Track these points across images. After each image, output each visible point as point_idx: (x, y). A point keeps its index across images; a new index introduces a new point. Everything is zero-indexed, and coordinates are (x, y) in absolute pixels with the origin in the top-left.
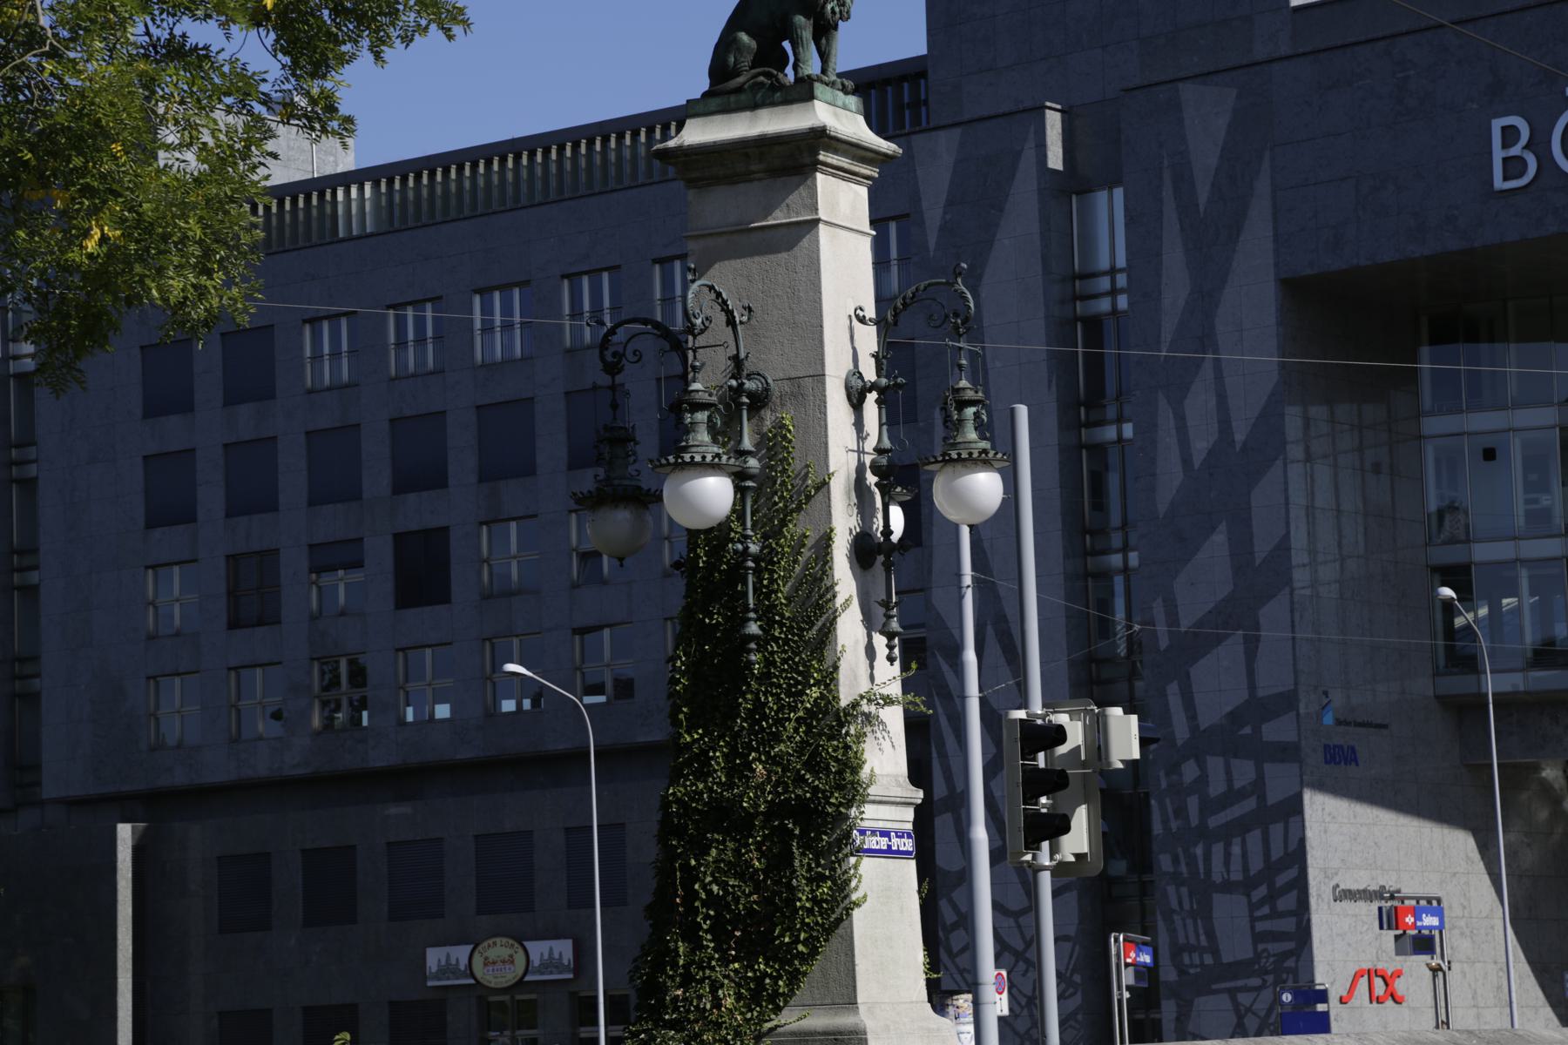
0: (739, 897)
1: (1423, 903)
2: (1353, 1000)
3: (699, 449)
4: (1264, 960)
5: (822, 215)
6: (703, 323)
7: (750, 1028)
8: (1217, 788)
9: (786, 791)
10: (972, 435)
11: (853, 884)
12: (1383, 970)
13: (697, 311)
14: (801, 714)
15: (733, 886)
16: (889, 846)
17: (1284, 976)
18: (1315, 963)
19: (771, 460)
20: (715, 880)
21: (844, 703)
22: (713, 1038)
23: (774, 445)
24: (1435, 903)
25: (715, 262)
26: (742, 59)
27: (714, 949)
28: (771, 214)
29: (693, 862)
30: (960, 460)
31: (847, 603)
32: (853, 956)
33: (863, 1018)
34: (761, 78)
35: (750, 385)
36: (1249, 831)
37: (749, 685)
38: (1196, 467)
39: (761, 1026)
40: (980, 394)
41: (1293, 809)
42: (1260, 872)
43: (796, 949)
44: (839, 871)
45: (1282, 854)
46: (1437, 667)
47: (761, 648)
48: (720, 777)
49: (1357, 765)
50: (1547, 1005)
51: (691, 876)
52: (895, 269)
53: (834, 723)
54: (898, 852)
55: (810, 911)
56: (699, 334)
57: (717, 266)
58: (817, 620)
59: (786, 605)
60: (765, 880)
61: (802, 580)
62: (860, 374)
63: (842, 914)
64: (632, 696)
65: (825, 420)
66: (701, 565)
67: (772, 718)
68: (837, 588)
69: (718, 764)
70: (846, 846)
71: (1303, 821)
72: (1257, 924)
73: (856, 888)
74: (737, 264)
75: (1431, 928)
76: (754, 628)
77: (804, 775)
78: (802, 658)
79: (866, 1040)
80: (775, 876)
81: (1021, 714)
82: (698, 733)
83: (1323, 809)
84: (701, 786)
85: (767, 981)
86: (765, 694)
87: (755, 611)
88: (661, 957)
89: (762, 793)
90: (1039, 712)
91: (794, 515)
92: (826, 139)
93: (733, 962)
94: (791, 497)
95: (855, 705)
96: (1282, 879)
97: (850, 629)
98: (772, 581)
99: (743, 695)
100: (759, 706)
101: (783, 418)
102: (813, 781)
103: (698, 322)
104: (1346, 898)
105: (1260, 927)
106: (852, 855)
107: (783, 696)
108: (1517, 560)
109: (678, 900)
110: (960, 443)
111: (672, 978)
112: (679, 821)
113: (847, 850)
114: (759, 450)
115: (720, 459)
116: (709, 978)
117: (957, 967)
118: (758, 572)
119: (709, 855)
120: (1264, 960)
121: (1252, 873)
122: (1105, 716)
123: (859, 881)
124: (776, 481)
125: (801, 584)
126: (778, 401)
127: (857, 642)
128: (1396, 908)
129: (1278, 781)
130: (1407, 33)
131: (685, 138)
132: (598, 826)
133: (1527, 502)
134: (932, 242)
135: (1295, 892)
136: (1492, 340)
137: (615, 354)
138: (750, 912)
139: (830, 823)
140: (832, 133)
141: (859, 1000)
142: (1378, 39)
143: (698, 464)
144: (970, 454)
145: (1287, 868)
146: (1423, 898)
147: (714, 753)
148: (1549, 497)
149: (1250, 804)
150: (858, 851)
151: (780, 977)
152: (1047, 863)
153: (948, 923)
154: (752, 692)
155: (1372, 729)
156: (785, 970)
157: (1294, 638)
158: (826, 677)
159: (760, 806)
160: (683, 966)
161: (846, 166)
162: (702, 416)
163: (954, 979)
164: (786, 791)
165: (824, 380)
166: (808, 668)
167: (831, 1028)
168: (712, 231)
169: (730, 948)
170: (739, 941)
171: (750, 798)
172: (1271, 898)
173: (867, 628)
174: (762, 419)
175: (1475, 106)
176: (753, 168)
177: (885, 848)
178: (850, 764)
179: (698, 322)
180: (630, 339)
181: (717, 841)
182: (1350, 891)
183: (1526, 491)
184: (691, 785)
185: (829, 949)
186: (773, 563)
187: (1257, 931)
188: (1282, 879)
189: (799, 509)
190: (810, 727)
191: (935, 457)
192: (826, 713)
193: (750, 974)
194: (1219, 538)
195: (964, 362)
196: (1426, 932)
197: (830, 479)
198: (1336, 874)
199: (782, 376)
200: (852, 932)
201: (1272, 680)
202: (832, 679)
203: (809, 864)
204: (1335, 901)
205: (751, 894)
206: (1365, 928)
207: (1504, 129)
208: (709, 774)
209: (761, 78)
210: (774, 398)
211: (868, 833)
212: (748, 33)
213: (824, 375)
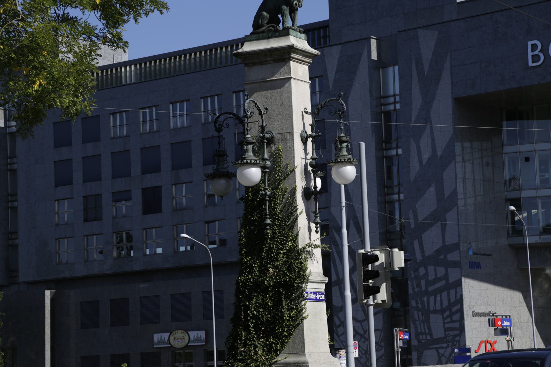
0: (263, 315)
1: (504, 317)
5: (292, 76)
7: (267, 362)
8: (431, 277)
9: (280, 278)
10: (345, 153)
11: (304, 311)
12: (490, 341)
13: (249, 110)
14: (285, 251)
15: (261, 312)
16: (316, 298)
18: (466, 339)
19: (274, 162)
20: (255, 310)
21: (300, 247)
23: (276, 157)
24: (508, 317)
25: (254, 93)
29: (247, 303)
30: (341, 162)
31: (301, 212)
32: (304, 336)
34: (271, 28)
36: (443, 292)
37: (267, 241)
38: (424, 164)
39: (271, 361)
40: (348, 139)
41: (459, 284)
42: (447, 306)
43: (284, 334)
44: (298, 306)
46: (509, 234)
48: (257, 274)
49: (481, 269)
51: (247, 308)
52: (318, 95)
53: (297, 254)
54: (319, 300)
55: (288, 321)
56: (249, 118)
57: (255, 94)
58: (291, 218)
59: (280, 213)
60: (273, 310)
62: (306, 131)
63: (300, 321)
65: (294, 148)
66: (250, 199)
67: (275, 253)
68: (298, 207)
69: (256, 269)
70: (301, 297)
71: (462, 288)
73: (305, 312)
74: (262, 93)
75: (507, 326)
76: (268, 221)
77: (286, 273)
78: (285, 232)
80: (276, 308)
81: (362, 251)
82: (249, 258)
84: (250, 277)
85: (274, 345)
86: (273, 244)
88: (236, 336)
90: (369, 250)
91: (283, 181)
92: (294, 49)
93: (262, 338)
94: (282, 175)
95: (304, 248)
96: (454, 309)
97: (302, 221)
98: (275, 204)
99: (265, 244)
100: (270, 248)
101: (279, 147)
102: (290, 275)
103: (249, 113)
104: (488, 316)
106: (303, 301)
107: (279, 245)
108: (536, 197)
109: (242, 317)
110: (341, 156)
111: (240, 344)
112: (242, 289)
113: (301, 299)
116: (253, 344)
117: (340, 340)
118: (270, 201)
119: (253, 301)
123: (306, 310)
125: (285, 205)
127: (305, 226)
128: (495, 319)
129: (453, 274)
130: (498, 11)
131: (244, 49)
132: (214, 291)
133: (540, 176)
134: (331, 86)
135: (459, 314)
137: (219, 125)
141: (306, 352)
142: (488, 14)
143: (249, 163)
144: (345, 160)
147: (255, 265)
149: (443, 282)
151: (278, 344)
152: (372, 303)
153: (337, 325)
154: (268, 244)
155: (486, 256)
156: (280, 341)
160: (244, 340)
161: (301, 58)
162: (250, 147)
163: (339, 344)
164: (280, 278)
165: (293, 134)
166: (288, 235)
169: (260, 334)
170: (263, 331)
171: (267, 281)
172: (451, 316)
173: (308, 221)
176: (268, 59)
177: (315, 298)
178: (303, 268)
179: (249, 113)
181: (256, 296)
182: (478, 313)
183: (540, 172)
184: (247, 276)
185: (295, 334)
186: (275, 198)
188: (454, 309)
189: (284, 179)
190: (288, 256)
191: (332, 161)
192: (294, 251)
193: (267, 343)
194: (432, 189)
195: (342, 127)
196: (505, 327)
197: (295, 168)
198: (473, 307)
199: (278, 132)
200: (303, 328)
201: (451, 239)
203: (288, 304)
204: (473, 316)
205: (268, 315)
206: (484, 326)
207: (532, 45)
208: (253, 272)
209: (271, 28)
210: (275, 140)
212: (266, 12)
213: (293, 132)
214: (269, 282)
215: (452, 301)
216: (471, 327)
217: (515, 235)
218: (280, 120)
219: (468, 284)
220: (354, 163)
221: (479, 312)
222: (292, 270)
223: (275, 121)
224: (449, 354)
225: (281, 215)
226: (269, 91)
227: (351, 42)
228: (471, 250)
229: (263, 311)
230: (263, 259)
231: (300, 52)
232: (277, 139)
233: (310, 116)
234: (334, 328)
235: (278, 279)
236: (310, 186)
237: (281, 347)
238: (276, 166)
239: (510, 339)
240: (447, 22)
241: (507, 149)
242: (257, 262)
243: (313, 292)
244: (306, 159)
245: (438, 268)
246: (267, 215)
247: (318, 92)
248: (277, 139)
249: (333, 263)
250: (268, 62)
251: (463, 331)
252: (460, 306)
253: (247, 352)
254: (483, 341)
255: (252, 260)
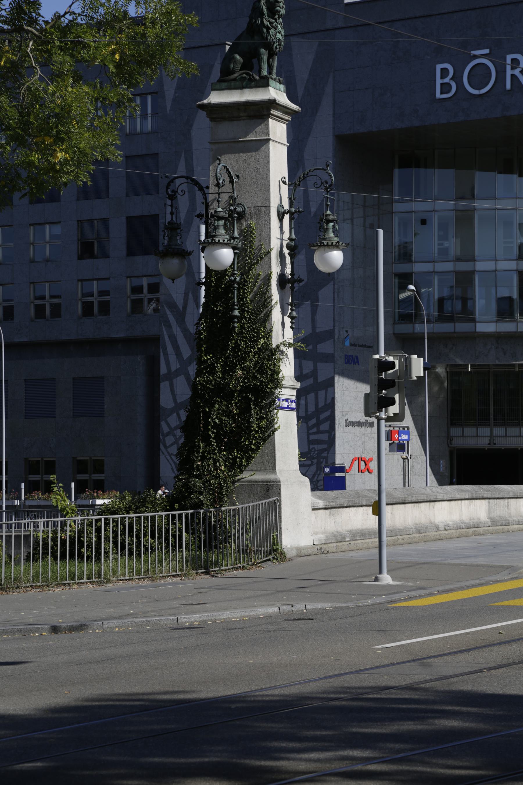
0: (227, 425)
1: (401, 429)
2: (351, 471)
3: (221, 237)
4: (313, 453)
5: (271, 137)
6: (222, 182)
7: (230, 479)
9: (249, 382)
10: (332, 235)
11: (276, 421)
12: (364, 458)
13: (220, 177)
14: (256, 350)
15: (225, 420)
16: (288, 406)
17: (322, 460)
18: (336, 454)
19: (245, 241)
20: (217, 418)
21: (274, 346)
22: (215, 482)
23: (247, 235)
24: (406, 429)
26: (237, 66)
27: (216, 446)
28: (248, 135)
29: (207, 410)
33: (278, 476)
34: (245, 75)
35: (239, 209)
36: (309, 394)
37: (233, 337)
39: (235, 478)
40: (336, 218)
41: (330, 384)
42: (313, 412)
43: (251, 447)
44: (270, 415)
45: (323, 404)
46: (395, 320)
47: (239, 321)
48: (219, 375)
49: (359, 364)
50: (432, 474)
51: (207, 415)
52: (149, 119)
53: (270, 354)
54: (291, 408)
55: (257, 432)
56: (221, 187)
58: (264, 311)
59: (250, 304)
60: (238, 418)
61: (257, 293)
62: (283, 206)
63: (270, 433)
64: (12, 319)
65: (270, 226)
66: (213, 285)
68: (273, 297)
69: (219, 369)
70: (273, 405)
71: (334, 390)
72: (310, 436)
73: (277, 423)
74: (232, 156)
75: (403, 440)
76: (236, 313)
77: (257, 375)
78: (256, 326)
79: (280, 485)
80: (242, 417)
81: (377, 357)
82: (210, 356)
83: (343, 384)
84: (211, 378)
85: (238, 460)
86: (240, 341)
87: (237, 305)
89: (238, 382)
90: (383, 356)
91: (256, 265)
92: (275, 105)
94: (254, 258)
95: (278, 347)
96: (322, 416)
97: (276, 314)
98: (244, 293)
99: (231, 340)
100: (237, 346)
101: (251, 224)
102: (261, 378)
103: (221, 181)
104: (351, 425)
105: (312, 437)
106: (276, 409)
107: (248, 342)
108: (433, 272)
109: (201, 425)
110: (327, 238)
111: (197, 457)
113: (273, 407)
114: (240, 237)
115: (230, 242)
116: (213, 458)
117: (168, 452)
118: (239, 289)
119: (215, 407)
120: (313, 453)
121: (309, 413)
122: (410, 359)
123: (278, 420)
124: (247, 251)
125: (257, 295)
126: (249, 216)
127: (279, 320)
128: (391, 431)
130: (399, 20)
131: (211, 100)
132: (5, 380)
133: (439, 244)
134: (169, 106)
135: (328, 422)
136: (426, 167)
137: (173, 191)
138: (232, 431)
139: (267, 395)
140: (278, 102)
141: (277, 468)
143: (221, 243)
144: (332, 243)
145: (326, 411)
146: (401, 427)
147: (217, 364)
148: (448, 243)
150: (278, 408)
151: (243, 458)
152: (384, 417)
154: (234, 340)
155: (365, 349)
156: (245, 456)
157: (334, 306)
158: (267, 335)
159: (237, 388)
160: (202, 453)
161: (280, 116)
162: (222, 222)
163: (167, 458)
164: (249, 382)
165: (270, 208)
166: (259, 331)
167: (265, 480)
168: (222, 141)
169: (222, 446)
170: (226, 442)
171: (233, 384)
172: (318, 424)
173: (282, 314)
174: (242, 224)
175: (429, 58)
176: (242, 115)
177: (286, 406)
178: (276, 371)
179: (221, 181)
180: (180, 185)
181: (218, 401)
182: (352, 422)
183: (439, 240)
184: (207, 377)
185: (265, 447)
186: (245, 286)
187: (310, 439)
188: (322, 416)
189: (257, 262)
190: (259, 355)
191: (317, 244)
192: (266, 350)
193: (230, 457)
195: (329, 203)
196: (401, 442)
197: (271, 251)
198: (347, 414)
199: (251, 205)
200: (274, 441)
202: (269, 336)
203: (257, 412)
204: (346, 426)
205: (232, 424)
206: (358, 439)
207: (442, 69)
208: (215, 373)
209: (245, 75)
210: (247, 215)
211: (281, 400)
212: (239, 55)
213: (270, 206)
214: (235, 386)
215: (320, 406)
216: (343, 440)
217: (402, 322)
218: (254, 190)
219: (342, 385)
220: (341, 248)
221: (353, 421)
222: (264, 372)
223: (248, 191)
224: (313, 474)
225: (252, 307)
226: (241, 154)
227: (199, 47)
228: (348, 340)
229: (226, 419)
230: (227, 358)
231: (281, 107)
232: (249, 213)
233: (287, 187)
234: (161, 437)
235: (246, 383)
236: (284, 272)
237: (246, 462)
238: (247, 246)
239: (407, 456)
240: (331, 29)
241: (398, 207)
242: (220, 361)
243: (290, 400)
244: (282, 239)
245: (304, 362)
246: (235, 305)
247: (150, 115)
248: (249, 213)
249: (162, 350)
250: (240, 118)
251: (332, 445)
252: (330, 412)
253: (205, 467)
254: (356, 458)
255: (214, 359)
